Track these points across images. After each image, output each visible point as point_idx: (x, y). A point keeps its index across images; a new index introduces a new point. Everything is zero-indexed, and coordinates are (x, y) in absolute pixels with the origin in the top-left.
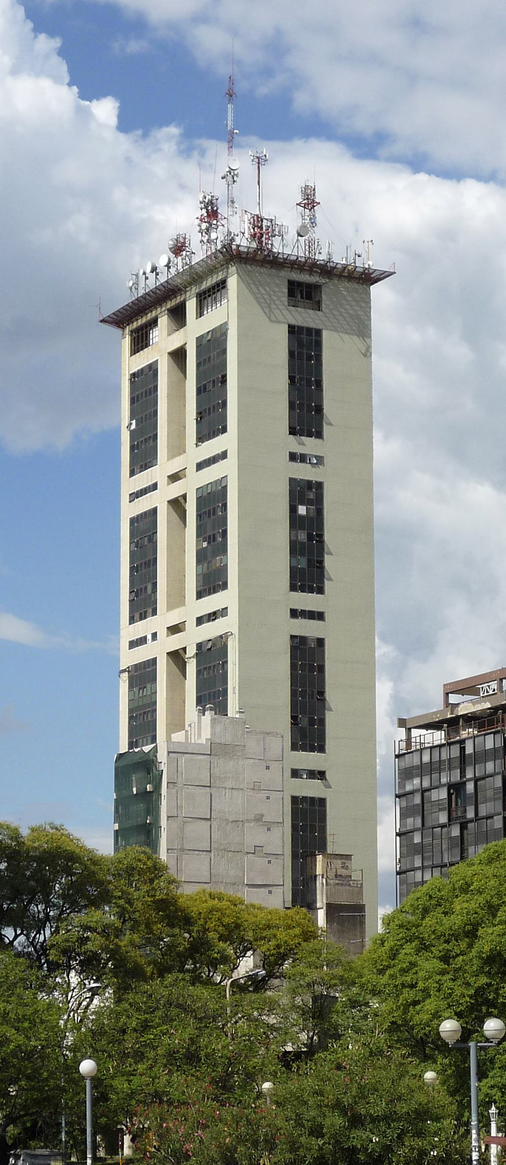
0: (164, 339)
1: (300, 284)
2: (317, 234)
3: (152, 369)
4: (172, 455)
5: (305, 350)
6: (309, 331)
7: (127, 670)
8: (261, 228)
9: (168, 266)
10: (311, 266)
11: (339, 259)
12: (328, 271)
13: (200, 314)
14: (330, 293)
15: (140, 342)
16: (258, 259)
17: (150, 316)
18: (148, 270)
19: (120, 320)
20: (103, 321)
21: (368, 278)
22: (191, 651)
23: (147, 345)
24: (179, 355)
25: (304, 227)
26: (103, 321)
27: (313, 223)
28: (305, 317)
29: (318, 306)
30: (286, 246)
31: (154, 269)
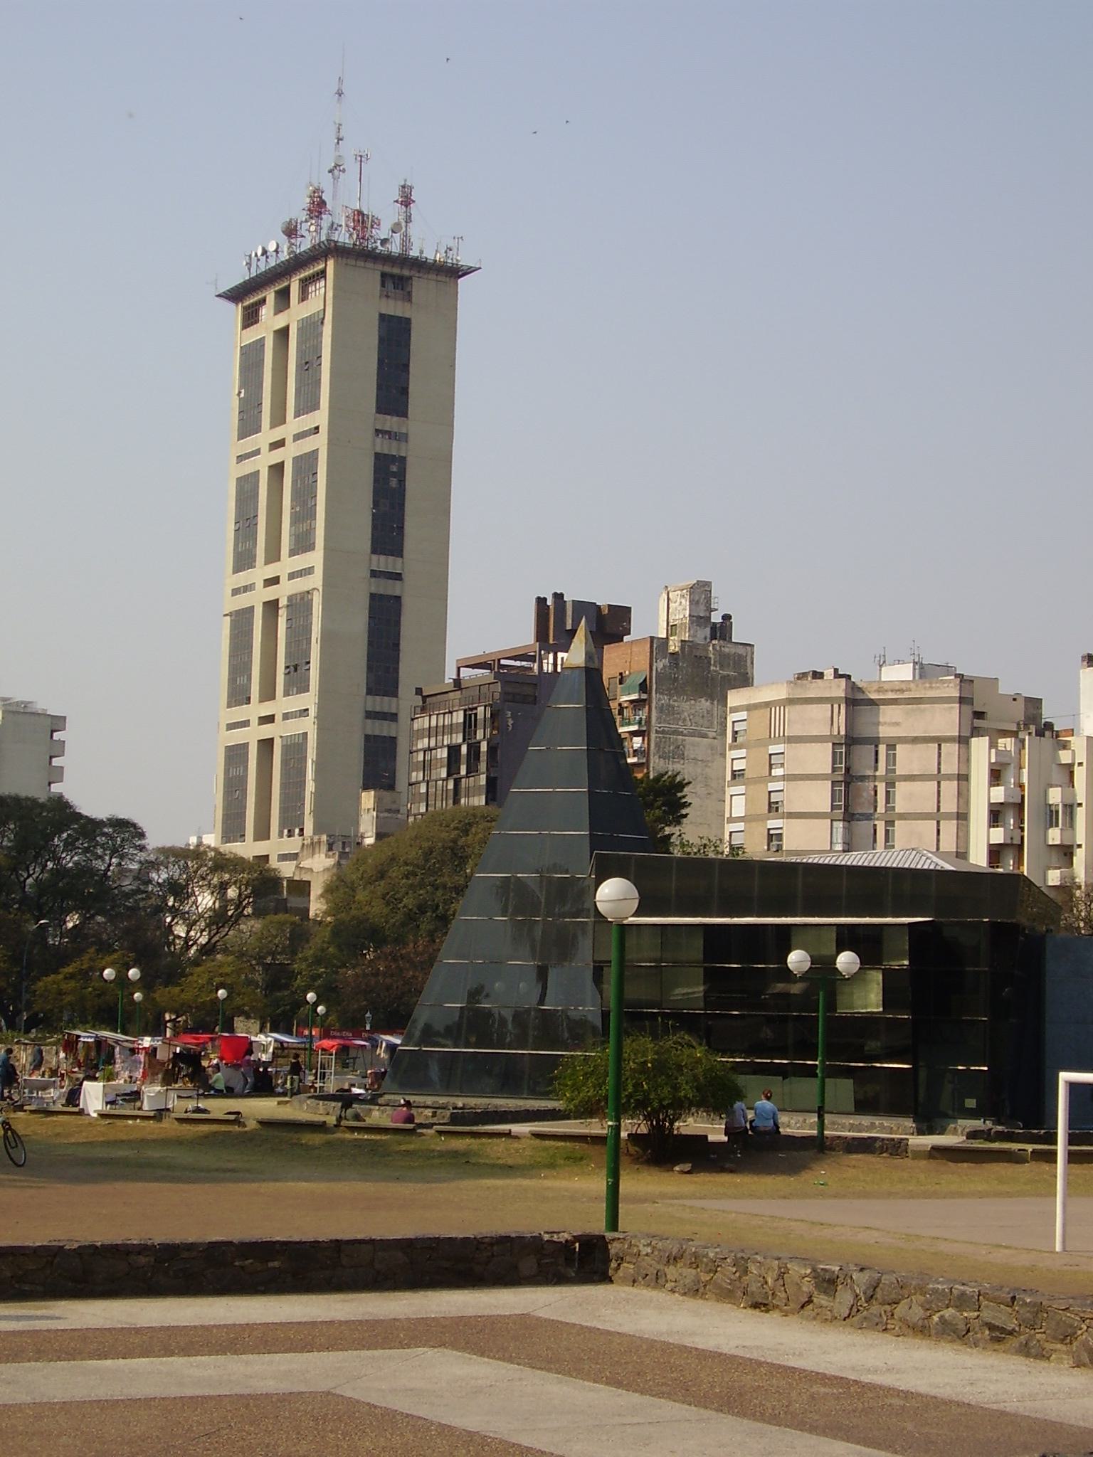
0: (270, 319)
1: (392, 276)
2: (414, 230)
3: (260, 343)
4: (273, 425)
5: (395, 341)
6: (390, 597)
7: (230, 614)
8: (361, 220)
9: (277, 251)
10: (404, 260)
11: (430, 255)
12: (420, 265)
13: (304, 297)
14: (422, 288)
15: (251, 318)
16: (357, 255)
17: (260, 297)
18: (259, 253)
19: (235, 295)
20: (219, 296)
21: (455, 272)
22: (283, 602)
23: (257, 322)
24: (283, 334)
25: (398, 224)
26: (219, 296)
27: (408, 219)
28: (395, 308)
29: (408, 297)
30: (382, 234)
31: (265, 252)
